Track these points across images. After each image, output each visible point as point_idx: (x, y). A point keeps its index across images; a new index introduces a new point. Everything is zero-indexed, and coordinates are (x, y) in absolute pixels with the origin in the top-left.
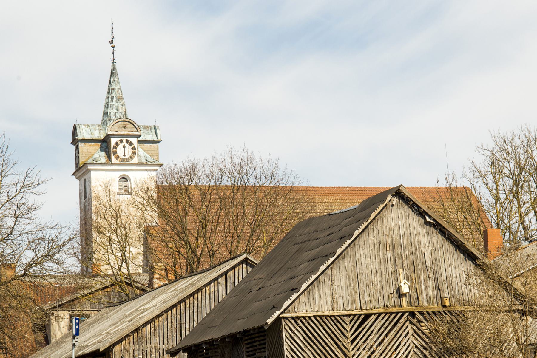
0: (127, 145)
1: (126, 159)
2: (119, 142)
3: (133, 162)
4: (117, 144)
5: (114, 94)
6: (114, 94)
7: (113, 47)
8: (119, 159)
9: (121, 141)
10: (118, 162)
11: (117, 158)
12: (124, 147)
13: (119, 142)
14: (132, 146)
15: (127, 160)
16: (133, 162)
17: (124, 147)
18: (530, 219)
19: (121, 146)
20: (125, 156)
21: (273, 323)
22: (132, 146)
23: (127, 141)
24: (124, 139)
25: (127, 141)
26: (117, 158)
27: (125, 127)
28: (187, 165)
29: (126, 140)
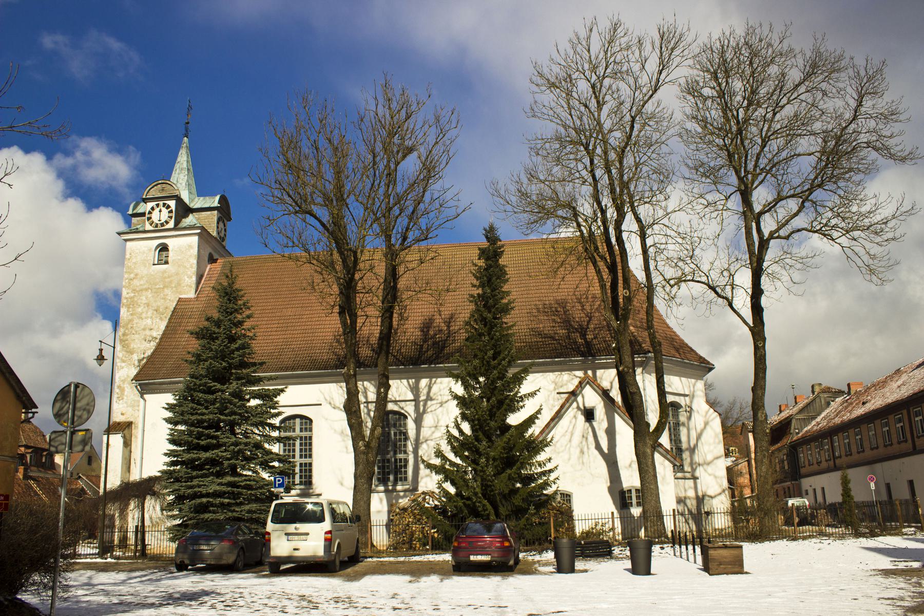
0: (164, 209)
9: (158, 205)
10: (151, 228)
13: (155, 206)
15: (162, 225)
16: (167, 227)
17: (160, 211)
19: (157, 210)
24: (161, 203)
25: (164, 205)
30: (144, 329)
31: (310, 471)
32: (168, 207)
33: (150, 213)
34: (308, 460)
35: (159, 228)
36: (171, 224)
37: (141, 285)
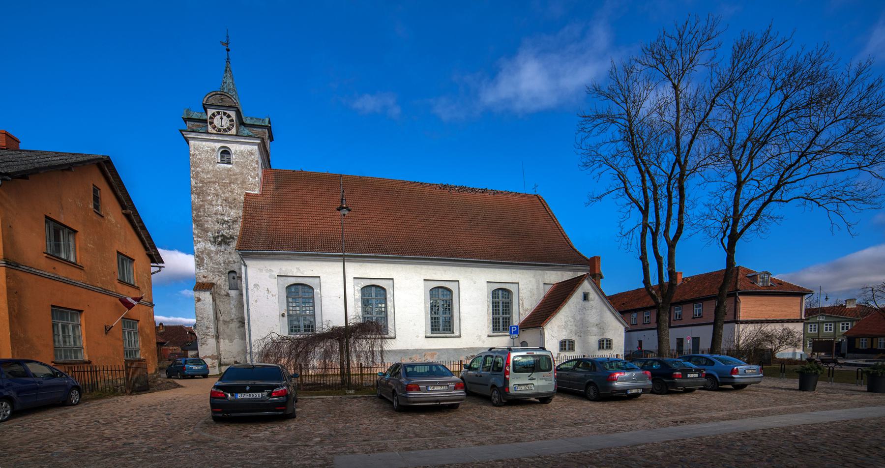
0: (225, 118)
1: (223, 129)
2: (216, 114)
3: (230, 133)
4: (214, 115)
5: (225, 86)
6: (225, 86)
7: (228, 50)
8: (216, 129)
9: (218, 113)
10: (214, 131)
11: (214, 127)
12: (221, 118)
14: (230, 119)
15: (225, 130)
16: (230, 133)
17: (221, 118)
18: (146, 467)
20: (222, 126)
21: (395, 251)
22: (230, 119)
23: (225, 114)
25: (225, 114)
26: (214, 127)
27: (222, 100)
28: (600, 351)
29: (224, 112)
30: (216, 214)
31: (432, 326)
32: (229, 116)
33: (211, 118)
34: (507, 316)
35: (221, 132)
36: (233, 131)
37: (208, 178)
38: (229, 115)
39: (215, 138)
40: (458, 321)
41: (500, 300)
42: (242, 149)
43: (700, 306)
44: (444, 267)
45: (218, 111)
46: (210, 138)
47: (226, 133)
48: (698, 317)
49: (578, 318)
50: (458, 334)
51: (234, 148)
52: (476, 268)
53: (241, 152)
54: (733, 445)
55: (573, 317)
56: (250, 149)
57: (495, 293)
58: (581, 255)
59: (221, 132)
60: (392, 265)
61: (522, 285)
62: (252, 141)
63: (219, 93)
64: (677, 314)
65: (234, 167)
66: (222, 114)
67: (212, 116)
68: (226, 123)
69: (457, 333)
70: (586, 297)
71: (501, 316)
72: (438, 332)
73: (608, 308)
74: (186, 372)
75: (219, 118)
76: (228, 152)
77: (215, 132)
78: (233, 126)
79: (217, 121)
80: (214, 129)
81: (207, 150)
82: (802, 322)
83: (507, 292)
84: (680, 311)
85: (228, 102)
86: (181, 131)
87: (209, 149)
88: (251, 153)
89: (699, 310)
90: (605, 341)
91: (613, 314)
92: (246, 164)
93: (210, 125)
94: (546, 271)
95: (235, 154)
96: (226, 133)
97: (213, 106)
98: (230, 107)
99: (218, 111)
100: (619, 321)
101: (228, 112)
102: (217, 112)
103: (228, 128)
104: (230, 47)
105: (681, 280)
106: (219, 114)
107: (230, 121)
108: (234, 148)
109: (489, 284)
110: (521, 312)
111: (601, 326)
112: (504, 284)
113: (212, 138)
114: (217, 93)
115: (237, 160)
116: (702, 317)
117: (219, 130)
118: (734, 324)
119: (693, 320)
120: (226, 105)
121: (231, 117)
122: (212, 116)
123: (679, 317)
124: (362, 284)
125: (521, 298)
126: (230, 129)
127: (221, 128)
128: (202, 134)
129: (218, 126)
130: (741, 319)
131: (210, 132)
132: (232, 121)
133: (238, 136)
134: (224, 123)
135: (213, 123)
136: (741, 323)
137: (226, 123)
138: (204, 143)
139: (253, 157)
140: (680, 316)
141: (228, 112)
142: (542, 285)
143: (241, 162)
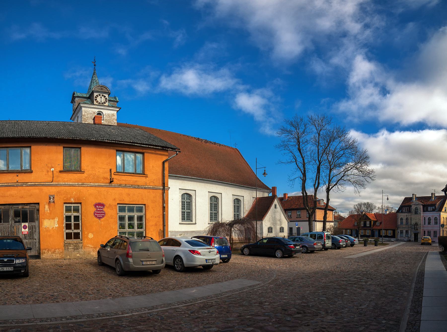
0: (103, 97)
1: (102, 103)
2: (98, 95)
3: (105, 105)
8: (98, 102)
9: (100, 95)
10: (97, 104)
11: (97, 102)
12: (101, 98)
14: (105, 98)
15: (102, 103)
16: (105, 105)
17: (101, 98)
20: (101, 101)
22: (105, 98)
23: (103, 95)
25: (103, 95)
26: (97, 102)
27: (102, 89)
29: (102, 95)
32: (105, 97)
35: (101, 104)
38: (105, 96)
39: (96, 107)
40: (221, 215)
41: (186, 200)
42: (109, 113)
43: (300, 212)
44: (216, 185)
45: (99, 94)
46: (94, 107)
47: (103, 105)
48: (299, 217)
49: (273, 216)
50: (194, 222)
51: (105, 112)
52: (229, 187)
53: (108, 115)
54: (117, 313)
55: (272, 216)
56: (113, 113)
57: (211, 198)
58: (264, 184)
59: (101, 104)
60: (195, 183)
61: (245, 197)
62: (115, 109)
63: (101, 86)
64: (298, 215)
65: (105, 122)
66: (102, 95)
67: (96, 96)
68: (103, 100)
69: (194, 222)
70: (275, 207)
71: (236, 213)
72: (189, 221)
73: (282, 212)
74: (341, 244)
75: (100, 97)
76: (101, 114)
77: (98, 104)
78: (107, 101)
79: (99, 99)
80: (97, 102)
81: (91, 113)
82: (333, 222)
83: (189, 196)
84: (291, 214)
85: (105, 90)
86: (121, 108)
87: (92, 112)
88: (113, 115)
89: (300, 214)
90: (270, 228)
91: (284, 215)
92: (110, 120)
93: (95, 100)
94: (254, 191)
95: (105, 115)
96: (103, 105)
97: (97, 92)
98: (105, 93)
99: (99, 94)
100: (286, 218)
101: (104, 95)
102: (99, 94)
103: (104, 102)
104: (96, 64)
105: (287, 198)
106: (100, 96)
107: (105, 99)
108: (105, 112)
109: (210, 193)
110: (245, 212)
111: (280, 220)
112: (215, 193)
113: (95, 107)
114: (100, 86)
115: (106, 118)
116: (301, 217)
117: (100, 103)
118: (315, 222)
119: (297, 218)
120: (104, 91)
121: (106, 97)
122: (96, 96)
123: (290, 217)
124: (182, 192)
125: (244, 204)
126: (105, 103)
127: (100, 102)
128: (90, 105)
129: (99, 101)
130: (317, 220)
131: (95, 104)
132: (106, 99)
133: (109, 106)
134: (102, 100)
135: (97, 100)
136: (317, 222)
137: (103, 100)
138: (90, 109)
139: (114, 117)
140: (290, 215)
141: (104, 95)
142: (252, 198)
143: (108, 119)
